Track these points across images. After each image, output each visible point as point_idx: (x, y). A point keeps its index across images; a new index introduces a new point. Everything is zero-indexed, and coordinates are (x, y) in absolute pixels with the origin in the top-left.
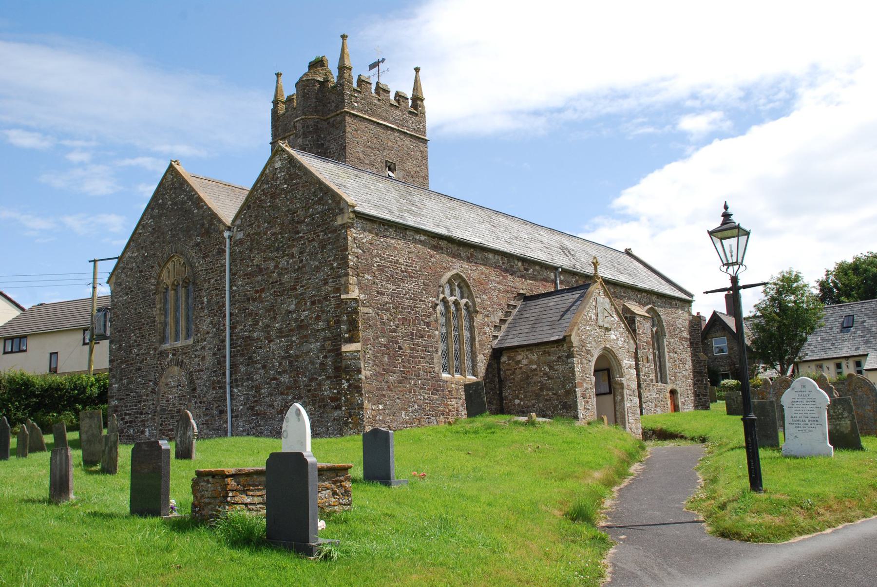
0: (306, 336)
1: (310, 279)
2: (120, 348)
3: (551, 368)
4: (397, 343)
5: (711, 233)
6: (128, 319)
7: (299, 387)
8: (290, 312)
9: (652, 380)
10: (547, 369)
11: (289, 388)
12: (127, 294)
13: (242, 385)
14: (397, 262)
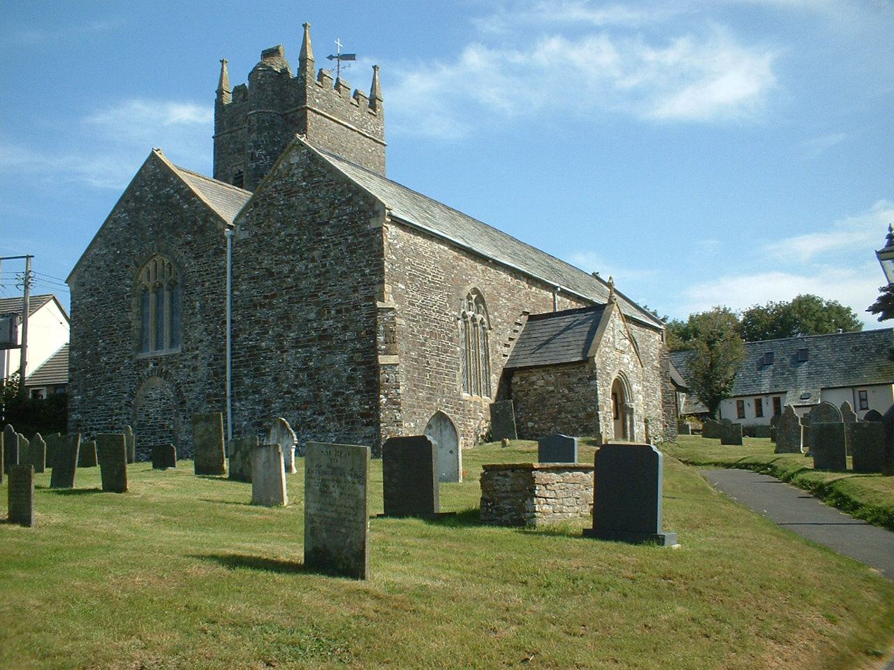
0: (329, 347)
1: (335, 285)
2: (84, 356)
3: (571, 390)
4: (426, 357)
5: (878, 253)
6: (94, 323)
7: (320, 402)
8: (309, 321)
10: (566, 391)
11: (306, 403)
12: (93, 295)
13: (246, 399)
14: (425, 271)
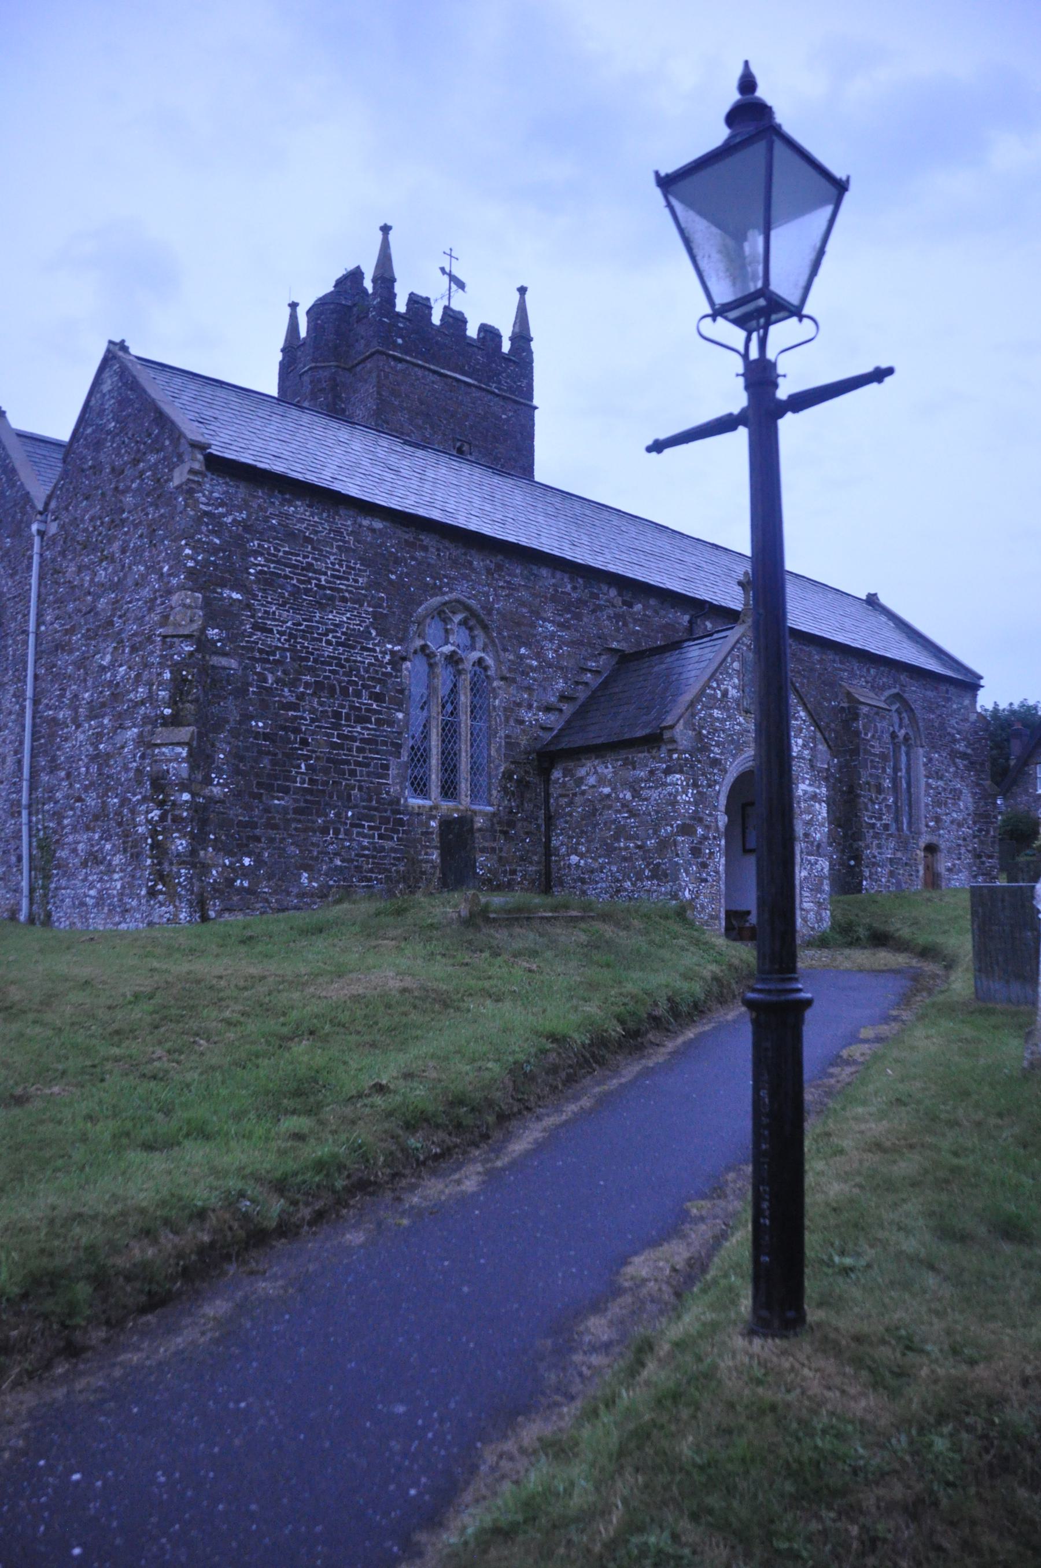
3: (636, 794)
4: (297, 731)
9: (886, 827)
10: (629, 796)
